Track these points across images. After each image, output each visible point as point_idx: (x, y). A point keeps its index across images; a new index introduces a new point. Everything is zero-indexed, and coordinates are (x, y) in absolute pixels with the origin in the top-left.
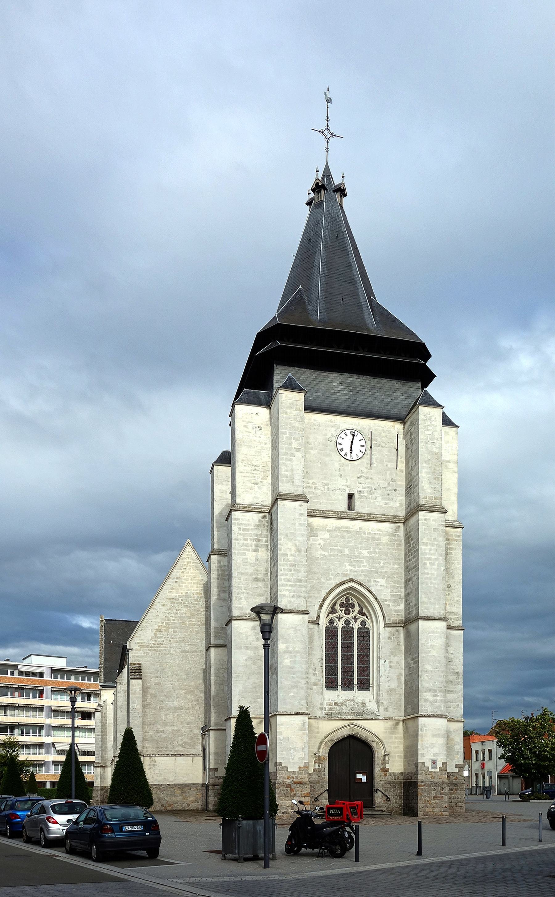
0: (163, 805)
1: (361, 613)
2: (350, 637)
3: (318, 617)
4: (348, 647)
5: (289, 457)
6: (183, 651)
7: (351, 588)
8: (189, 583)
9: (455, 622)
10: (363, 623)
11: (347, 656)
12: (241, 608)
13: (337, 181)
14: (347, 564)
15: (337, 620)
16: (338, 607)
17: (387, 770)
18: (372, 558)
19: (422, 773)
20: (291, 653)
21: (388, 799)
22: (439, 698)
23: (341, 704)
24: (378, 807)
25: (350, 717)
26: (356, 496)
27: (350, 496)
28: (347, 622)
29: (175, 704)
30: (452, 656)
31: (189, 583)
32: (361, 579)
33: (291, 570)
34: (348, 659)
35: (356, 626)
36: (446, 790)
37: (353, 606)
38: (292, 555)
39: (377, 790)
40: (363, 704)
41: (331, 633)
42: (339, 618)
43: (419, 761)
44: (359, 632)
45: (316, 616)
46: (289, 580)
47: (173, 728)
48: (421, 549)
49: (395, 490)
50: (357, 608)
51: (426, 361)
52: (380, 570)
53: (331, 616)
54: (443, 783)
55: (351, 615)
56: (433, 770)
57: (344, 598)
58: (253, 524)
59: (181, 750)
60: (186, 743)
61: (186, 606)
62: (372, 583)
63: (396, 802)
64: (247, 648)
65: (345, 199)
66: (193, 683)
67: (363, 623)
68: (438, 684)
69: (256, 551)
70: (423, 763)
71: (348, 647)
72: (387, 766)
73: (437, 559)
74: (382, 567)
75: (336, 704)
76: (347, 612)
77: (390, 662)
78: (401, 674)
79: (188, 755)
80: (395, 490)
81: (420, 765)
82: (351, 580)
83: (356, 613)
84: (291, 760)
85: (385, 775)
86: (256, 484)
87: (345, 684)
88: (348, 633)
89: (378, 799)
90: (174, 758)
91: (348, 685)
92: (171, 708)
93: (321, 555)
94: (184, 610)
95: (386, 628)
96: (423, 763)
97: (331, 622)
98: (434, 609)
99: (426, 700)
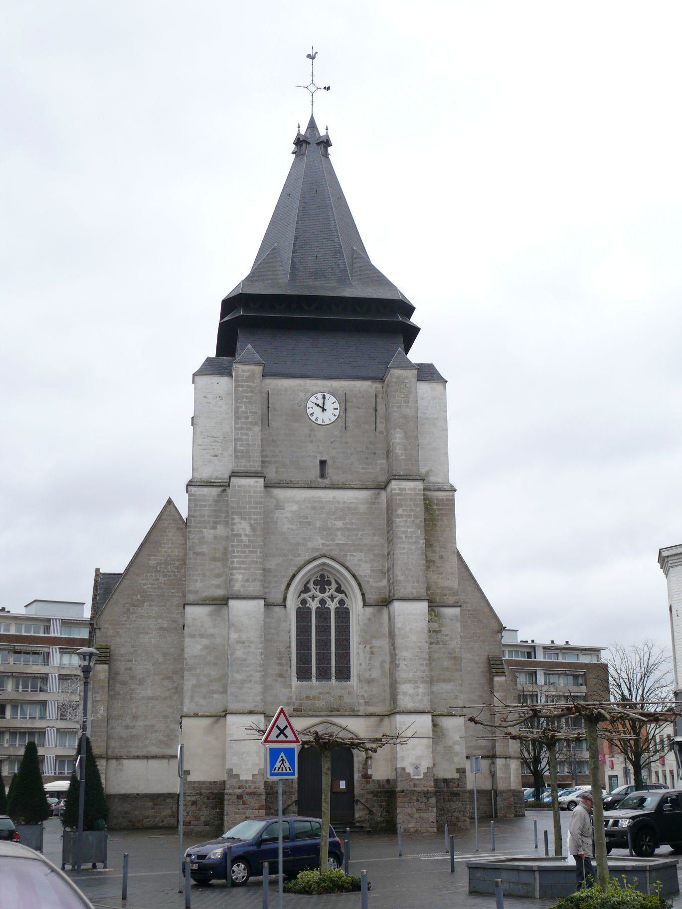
0: (130, 821)
1: (339, 590)
2: (326, 619)
3: (285, 599)
4: (323, 630)
5: (244, 432)
6: (161, 629)
7: (324, 564)
8: (169, 548)
9: (450, 598)
10: (342, 602)
11: (323, 641)
12: (196, 592)
13: (322, 132)
14: (319, 538)
15: (310, 600)
16: (311, 585)
17: (370, 777)
18: (348, 529)
19: (402, 781)
20: (244, 643)
21: (371, 812)
22: (420, 691)
23: (314, 697)
24: (358, 822)
25: (322, 714)
26: (329, 463)
27: (323, 463)
28: (323, 602)
29: (149, 693)
30: (447, 638)
31: (169, 548)
32: (334, 553)
33: (245, 552)
34: (323, 644)
35: (332, 606)
36: (433, 800)
37: (329, 583)
38: (246, 535)
39: (357, 801)
40: (341, 697)
41: (303, 614)
42: (313, 598)
43: (399, 766)
44: (336, 613)
45: (282, 597)
46: (243, 563)
47: (146, 723)
48: (239, 591)
49: (375, 454)
50: (334, 586)
51: (409, 316)
52: (357, 543)
53: (304, 596)
54: (428, 792)
55: (327, 594)
56: (416, 777)
57: (319, 574)
58: (211, 499)
59: (154, 750)
60: (161, 741)
61: (165, 576)
62: (349, 558)
63: (381, 816)
64: (202, 636)
65: (329, 148)
66: (171, 667)
67: (342, 602)
68: (419, 674)
69: (214, 528)
70: (404, 769)
71: (323, 630)
72: (370, 772)
73: (413, 533)
74: (360, 539)
75: (308, 697)
76: (323, 591)
77: (371, 648)
78: (384, 661)
79: (163, 757)
80: (375, 454)
81: (399, 771)
82: (324, 556)
83: (332, 591)
84: (243, 767)
85: (368, 782)
86: (216, 456)
87: (321, 674)
88: (323, 613)
89: (359, 813)
90: (145, 761)
91: (324, 674)
92: (144, 697)
93: (289, 529)
94: (162, 579)
95: (366, 608)
96: (404, 769)
97: (304, 602)
98: (413, 588)
99: (405, 694)
